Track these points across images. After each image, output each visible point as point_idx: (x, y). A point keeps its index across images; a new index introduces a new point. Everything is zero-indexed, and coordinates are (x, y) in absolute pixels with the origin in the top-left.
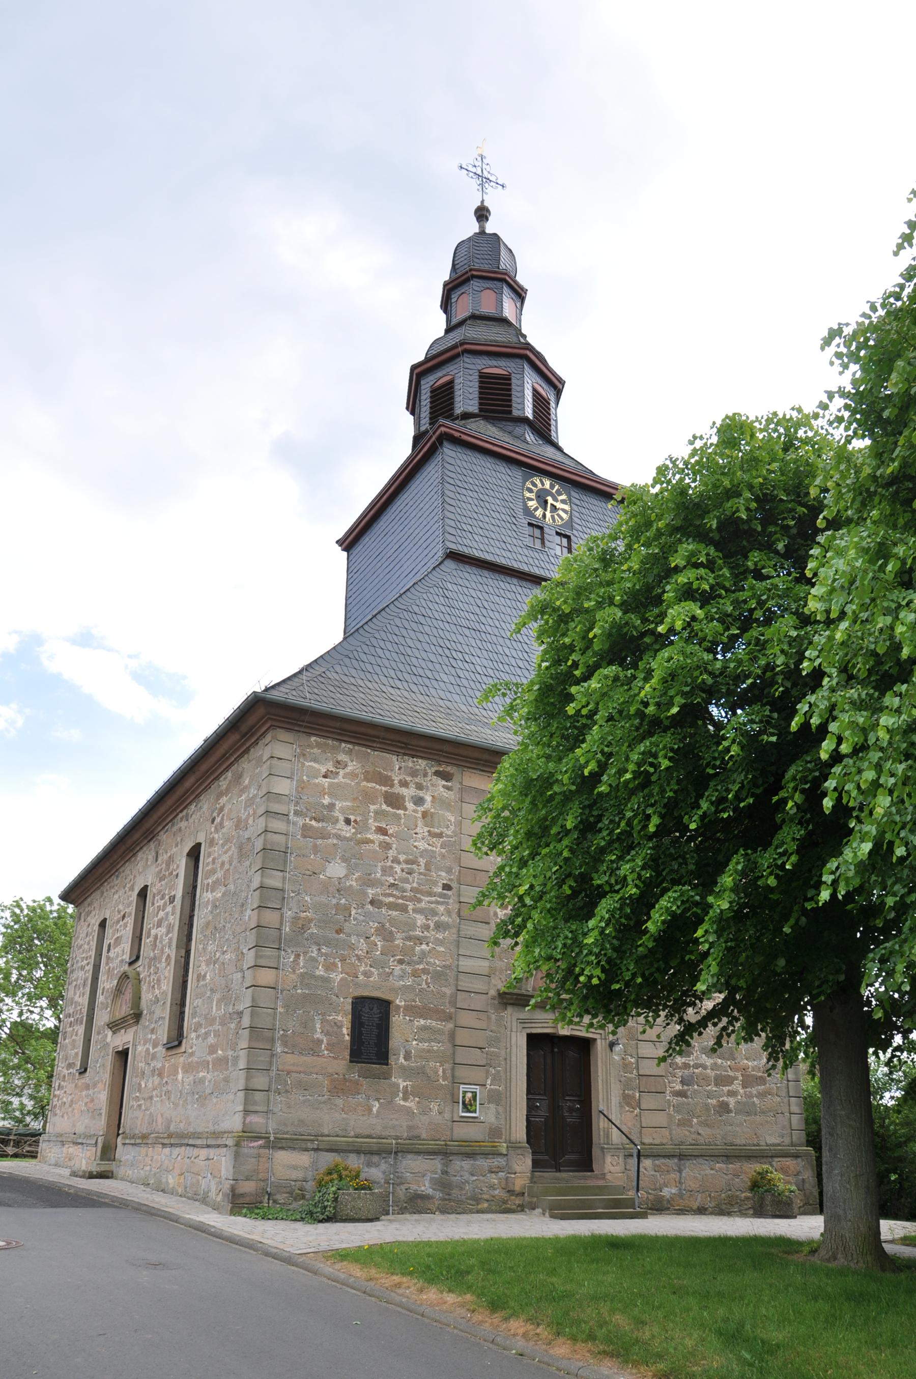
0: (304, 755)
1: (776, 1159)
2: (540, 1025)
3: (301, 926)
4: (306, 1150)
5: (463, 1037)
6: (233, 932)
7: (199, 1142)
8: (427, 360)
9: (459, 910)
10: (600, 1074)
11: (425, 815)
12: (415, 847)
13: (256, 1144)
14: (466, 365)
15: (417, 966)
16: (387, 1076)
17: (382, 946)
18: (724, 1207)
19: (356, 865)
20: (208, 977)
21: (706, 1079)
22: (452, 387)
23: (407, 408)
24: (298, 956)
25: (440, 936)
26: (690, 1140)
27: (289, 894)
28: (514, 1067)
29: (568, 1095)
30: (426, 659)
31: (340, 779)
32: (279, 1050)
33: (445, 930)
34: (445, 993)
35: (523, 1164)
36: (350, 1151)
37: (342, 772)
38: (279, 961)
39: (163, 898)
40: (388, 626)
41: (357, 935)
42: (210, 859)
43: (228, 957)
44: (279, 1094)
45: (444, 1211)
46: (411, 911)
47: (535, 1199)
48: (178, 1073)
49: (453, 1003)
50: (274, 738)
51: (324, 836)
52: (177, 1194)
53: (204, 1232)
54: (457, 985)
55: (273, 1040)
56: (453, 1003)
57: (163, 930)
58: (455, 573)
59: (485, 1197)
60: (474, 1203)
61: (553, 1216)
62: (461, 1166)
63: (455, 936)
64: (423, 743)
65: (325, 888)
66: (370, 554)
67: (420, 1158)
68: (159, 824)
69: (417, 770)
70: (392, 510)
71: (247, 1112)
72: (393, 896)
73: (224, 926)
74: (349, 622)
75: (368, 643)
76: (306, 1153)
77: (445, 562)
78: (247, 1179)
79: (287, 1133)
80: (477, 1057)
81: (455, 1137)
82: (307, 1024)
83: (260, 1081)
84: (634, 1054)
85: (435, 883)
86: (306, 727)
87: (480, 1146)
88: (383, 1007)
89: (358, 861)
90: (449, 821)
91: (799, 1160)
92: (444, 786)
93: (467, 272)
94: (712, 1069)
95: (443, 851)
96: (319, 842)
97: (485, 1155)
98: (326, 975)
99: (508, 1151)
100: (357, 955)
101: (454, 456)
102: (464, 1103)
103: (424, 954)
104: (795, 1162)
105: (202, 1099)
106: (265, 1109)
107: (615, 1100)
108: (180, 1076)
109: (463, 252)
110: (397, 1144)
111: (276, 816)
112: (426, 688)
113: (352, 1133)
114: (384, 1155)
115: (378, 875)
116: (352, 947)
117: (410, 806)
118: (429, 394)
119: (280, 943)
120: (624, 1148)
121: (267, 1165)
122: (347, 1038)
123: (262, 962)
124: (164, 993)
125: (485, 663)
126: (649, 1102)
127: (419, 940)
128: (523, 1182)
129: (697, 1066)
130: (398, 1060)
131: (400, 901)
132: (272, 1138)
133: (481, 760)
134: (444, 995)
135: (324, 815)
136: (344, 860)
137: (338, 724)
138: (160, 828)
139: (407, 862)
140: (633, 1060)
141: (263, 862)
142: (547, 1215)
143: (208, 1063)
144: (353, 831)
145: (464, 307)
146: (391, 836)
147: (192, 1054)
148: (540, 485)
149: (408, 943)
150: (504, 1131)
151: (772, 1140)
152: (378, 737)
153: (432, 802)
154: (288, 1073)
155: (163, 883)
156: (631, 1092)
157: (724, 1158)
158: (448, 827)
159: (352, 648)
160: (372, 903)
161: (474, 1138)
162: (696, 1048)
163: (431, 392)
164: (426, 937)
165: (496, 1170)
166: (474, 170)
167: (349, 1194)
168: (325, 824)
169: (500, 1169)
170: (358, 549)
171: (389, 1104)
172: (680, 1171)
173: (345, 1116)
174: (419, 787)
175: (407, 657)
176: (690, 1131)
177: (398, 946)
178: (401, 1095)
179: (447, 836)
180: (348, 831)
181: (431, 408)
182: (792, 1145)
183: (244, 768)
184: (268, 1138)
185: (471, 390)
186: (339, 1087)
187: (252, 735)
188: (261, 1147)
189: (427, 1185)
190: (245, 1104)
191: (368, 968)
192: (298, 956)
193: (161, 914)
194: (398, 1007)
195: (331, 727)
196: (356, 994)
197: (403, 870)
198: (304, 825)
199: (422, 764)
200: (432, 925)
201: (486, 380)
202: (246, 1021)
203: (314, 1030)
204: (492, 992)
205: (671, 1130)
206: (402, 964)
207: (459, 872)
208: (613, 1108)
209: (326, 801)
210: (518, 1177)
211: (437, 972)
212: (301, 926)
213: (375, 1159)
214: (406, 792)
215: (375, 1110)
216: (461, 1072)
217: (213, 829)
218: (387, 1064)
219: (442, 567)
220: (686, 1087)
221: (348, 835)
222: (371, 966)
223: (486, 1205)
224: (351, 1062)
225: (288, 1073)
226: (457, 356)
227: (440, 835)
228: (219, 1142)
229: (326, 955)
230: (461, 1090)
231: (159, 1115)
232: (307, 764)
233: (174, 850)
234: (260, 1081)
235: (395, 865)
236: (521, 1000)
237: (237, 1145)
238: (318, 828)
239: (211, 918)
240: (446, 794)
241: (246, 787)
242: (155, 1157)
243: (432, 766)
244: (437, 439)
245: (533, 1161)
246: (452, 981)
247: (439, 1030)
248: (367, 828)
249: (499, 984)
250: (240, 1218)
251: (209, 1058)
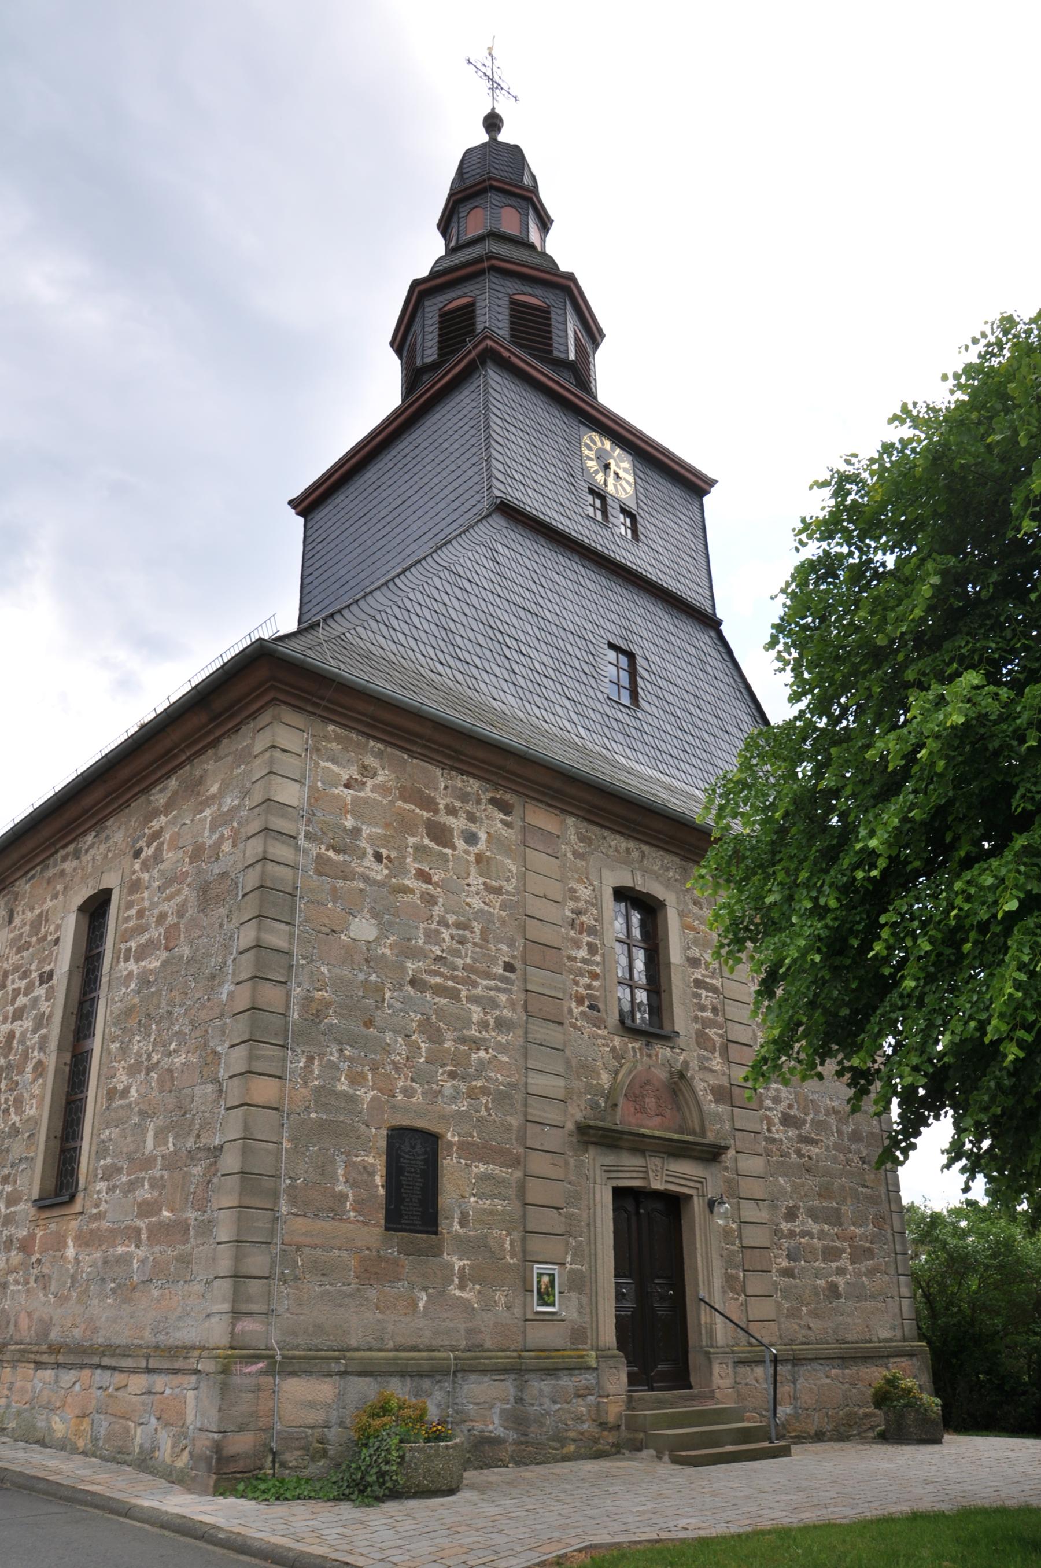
0: (318, 750)
1: (892, 1360)
2: (628, 1175)
3: (315, 1013)
4: (329, 1375)
5: (536, 1192)
6: (191, 1021)
7: (128, 1363)
8: (434, 274)
9: (526, 1001)
10: (698, 1246)
11: (479, 858)
12: (468, 904)
13: (253, 1368)
14: (494, 286)
15: (474, 1083)
16: (436, 1252)
17: (428, 1050)
18: (842, 1429)
19: (391, 924)
20: (133, 1092)
21: (813, 1251)
22: (474, 311)
23: (392, 344)
24: (310, 1059)
25: (502, 1039)
26: (800, 1336)
27: (297, 961)
28: (599, 1236)
29: (658, 1277)
30: (473, 639)
31: (367, 793)
32: (284, 1210)
33: (509, 1030)
34: (510, 1125)
35: (617, 1380)
36: (391, 1374)
37: (370, 783)
38: (284, 1067)
39: (25, 975)
40: (425, 585)
41: (394, 1031)
42: (133, 912)
43: (179, 1060)
44: (285, 1282)
45: (521, 1461)
46: (464, 999)
47: (641, 1435)
48: (65, 1246)
49: (522, 1139)
50: (277, 718)
51: (347, 875)
52: (74, 1450)
53: (201, 1538)
54: (526, 1114)
55: (275, 1195)
56: (522, 1139)
57: (28, 1024)
58: (504, 530)
59: (572, 1434)
60: (558, 1445)
61: (676, 1461)
62: (540, 1387)
63: (521, 1040)
64: (480, 754)
65: (349, 952)
66: (347, 517)
67: (486, 1379)
68: (18, 869)
69: (468, 794)
70: (389, 457)
71: (236, 1314)
72: (441, 975)
73: (170, 1013)
74: (305, 609)
75: (400, 604)
76: (328, 1379)
77: (494, 516)
78: (241, 1429)
79: (296, 1347)
80: (553, 1221)
81: (530, 1345)
82: (325, 1169)
83: (257, 1262)
85: (494, 960)
86: (326, 708)
87: (563, 1357)
88: (430, 1140)
89: (393, 918)
90: (510, 871)
91: (914, 1359)
92: (502, 821)
93: (484, 181)
94: (819, 1239)
95: (504, 914)
96: (340, 884)
97: (570, 1370)
98: (351, 1091)
99: (598, 1362)
100: (393, 1062)
101: (500, 382)
102: (539, 1290)
103: (482, 1065)
104: (910, 1363)
105: (126, 1291)
106: (264, 1308)
107: (718, 1282)
108: (71, 1252)
109: (475, 159)
110: (455, 1358)
111: (280, 837)
112: (474, 681)
113: (391, 1345)
114: (438, 1378)
115: (421, 942)
116: (387, 1050)
117: (460, 844)
118: (436, 318)
119: (286, 1038)
120: (733, 1352)
121: (270, 1404)
122: (382, 1191)
123: (258, 1066)
124: (34, 1121)
125: (545, 659)
126: (755, 1285)
127: (476, 1044)
128: (617, 1409)
129: (804, 1234)
130: (452, 1226)
131: (450, 983)
132: (279, 1358)
133: (549, 788)
134: (509, 1128)
135: (346, 843)
136: (375, 914)
137: (371, 709)
138: (21, 873)
139: (458, 926)
140: (734, 1226)
141: (261, 907)
142: (666, 1458)
143: (138, 1231)
144: (386, 872)
145: (475, 223)
146: (436, 885)
147: (99, 1216)
148: (599, 444)
149: (462, 1047)
150: (589, 1334)
151: (884, 1334)
152: (421, 737)
153: (487, 841)
154: (298, 1248)
155: (25, 954)
156: (734, 1271)
157: (840, 1361)
158: (508, 880)
159: (381, 608)
160: (413, 982)
161: (553, 1346)
162: (802, 1210)
163: (440, 316)
164: (484, 1040)
166: (483, 69)
167: (420, 1450)
168: (347, 858)
169: (589, 1390)
170: (319, 515)
171: (440, 1297)
172: (794, 1382)
173: (380, 1316)
174: (471, 818)
175: (449, 633)
176: (799, 1325)
177: (448, 1050)
178: (456, 1281)
179: (508, 893)
180: (379, 872)
181: (440, 335)
182: (904, 1339)
183: (206, 771)
184: (273, 1357)
185: (500, 317)
186: (374, 1270)
187: (231, 717)
188: (261, 1373)
189: (496, 1422)
190: (234, 1301)
191: (409, 1083)
192: (310, 1059)
193: (21, 1001)
194: (450, 1144)
195: (359, 713)
196: (393, 1123)
197: (452, 938)
198: (319, 856)
199: (473, 785)
200: (492, 1022)
201: (519, 312)
202: (231, 1161)
203: (334, 1179)
204: (570, 1126)
205: (779, 1324)
206: (454, 1078)
207: (525, 946)
209: (349, 822)
211: (500, 1093)
212: (315, 1013)
213: (426, 1383)
214: (457, 824)
215: (421, 1305)
216: (536, 1244)
217: (137, 867)
218: (436, 1233)
219: (489, 520)
220: (793, 1264)
221: (379, 878)
222: (413, 1080)
223: (572, 1447)
224: (387, 1229)
225: (298, 1248)
226: (482, 272)
227: (498, 891)
228: (179, 1364)
229: (350, 1059)
230: (535, 1271)
231: (23, 1315)
232: (323, 764)
233: (49, 904)
234: (257, 1262)
235: (442, 929)
237: (225, 1371)
238: (338, 862)
239: (136, 1000)
240: (505, 832)
241: (214, 797)
242: (18, 1384)
243: (487, 790)
244: (479, 356)
245: (630, 1375)
246: (519, 1106)
247: (504, 1180)
248: (405, 872)
249: (577, 1113)
250: (232, 1500)
251: (141, 1224)
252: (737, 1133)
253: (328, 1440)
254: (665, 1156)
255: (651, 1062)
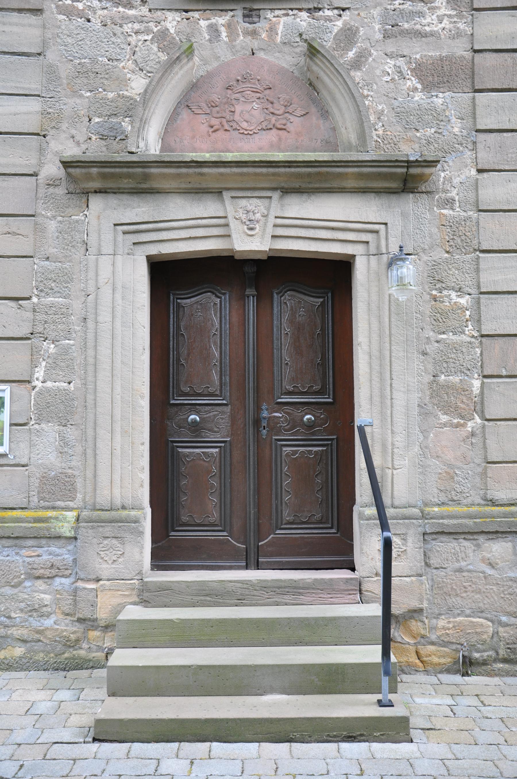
59: (16, 632)
84: (468, 282)
120: (424, 516)
140: (464, 301)
150: (79, 485)
156: (455, 379)
165: (47, 573)
208: (400, 419)
210: (104, 589)
236: (113, 176)
252: (482, 137)
253: (102, 577)
254: (276, 195)
255: (255, 44)
